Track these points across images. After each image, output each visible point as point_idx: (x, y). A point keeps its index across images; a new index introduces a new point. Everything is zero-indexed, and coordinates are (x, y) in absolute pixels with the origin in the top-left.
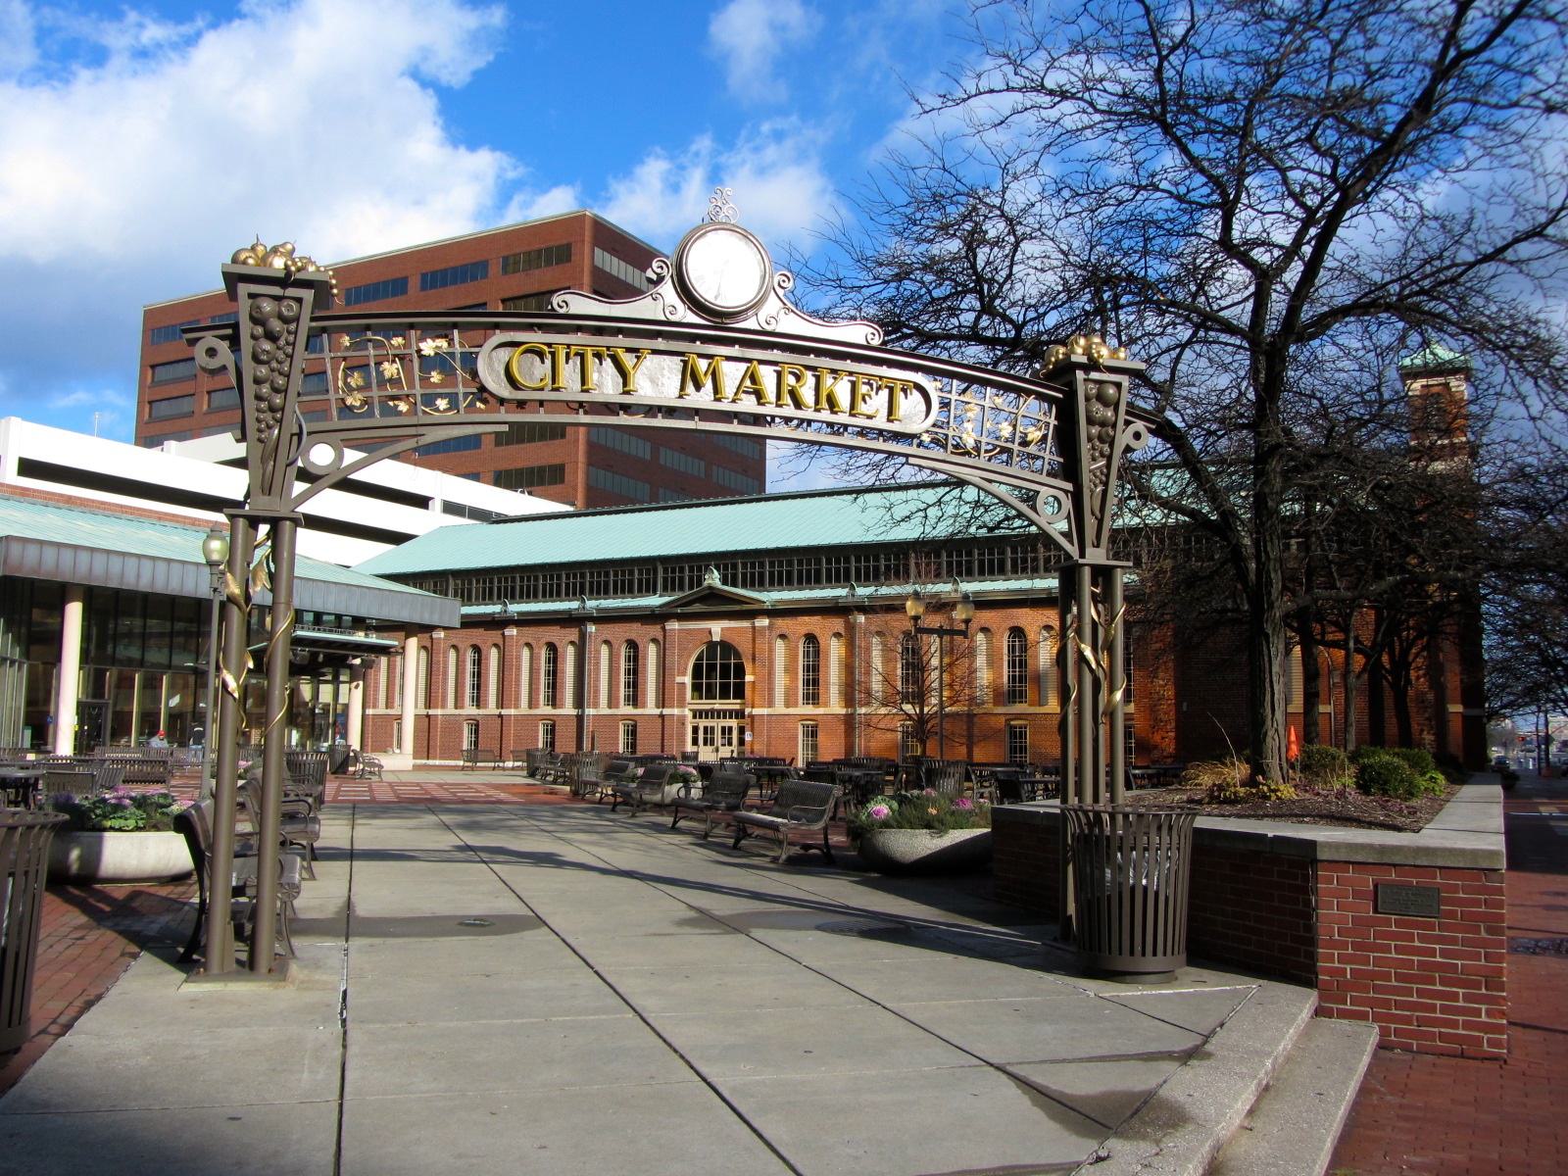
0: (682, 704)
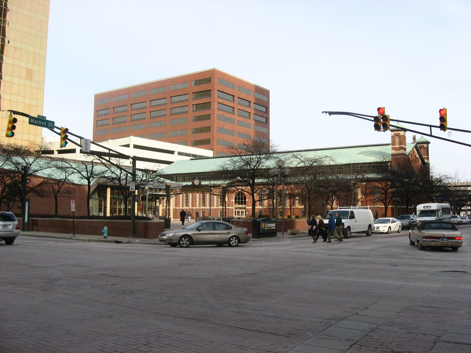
0: (232, 206)
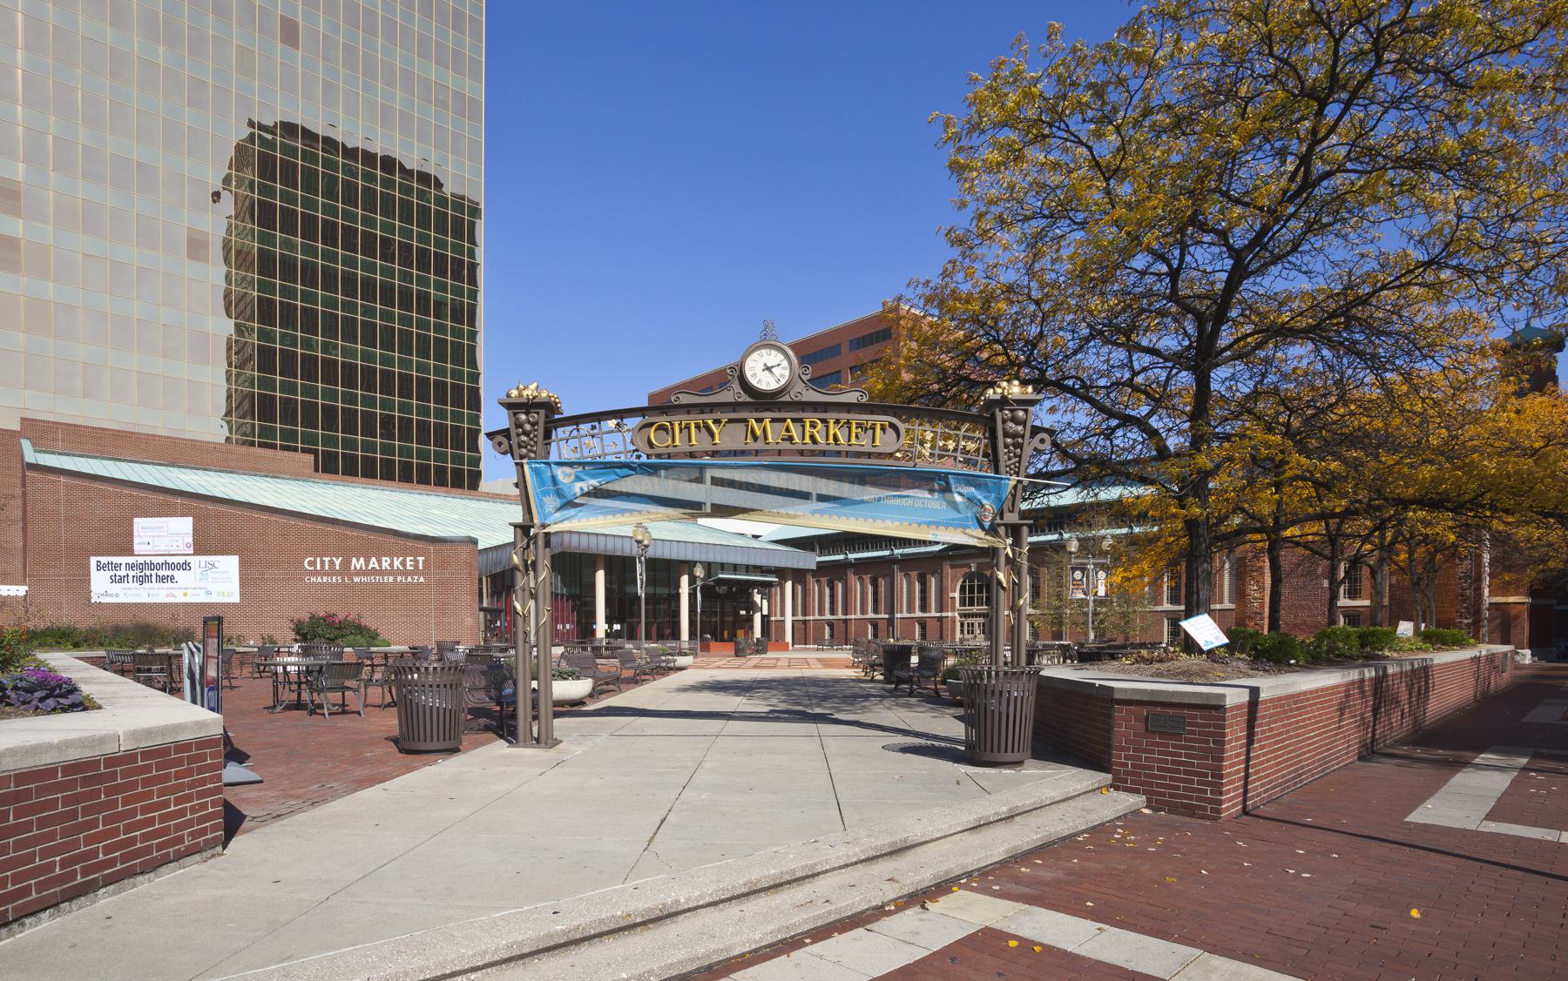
0: (953, 610)
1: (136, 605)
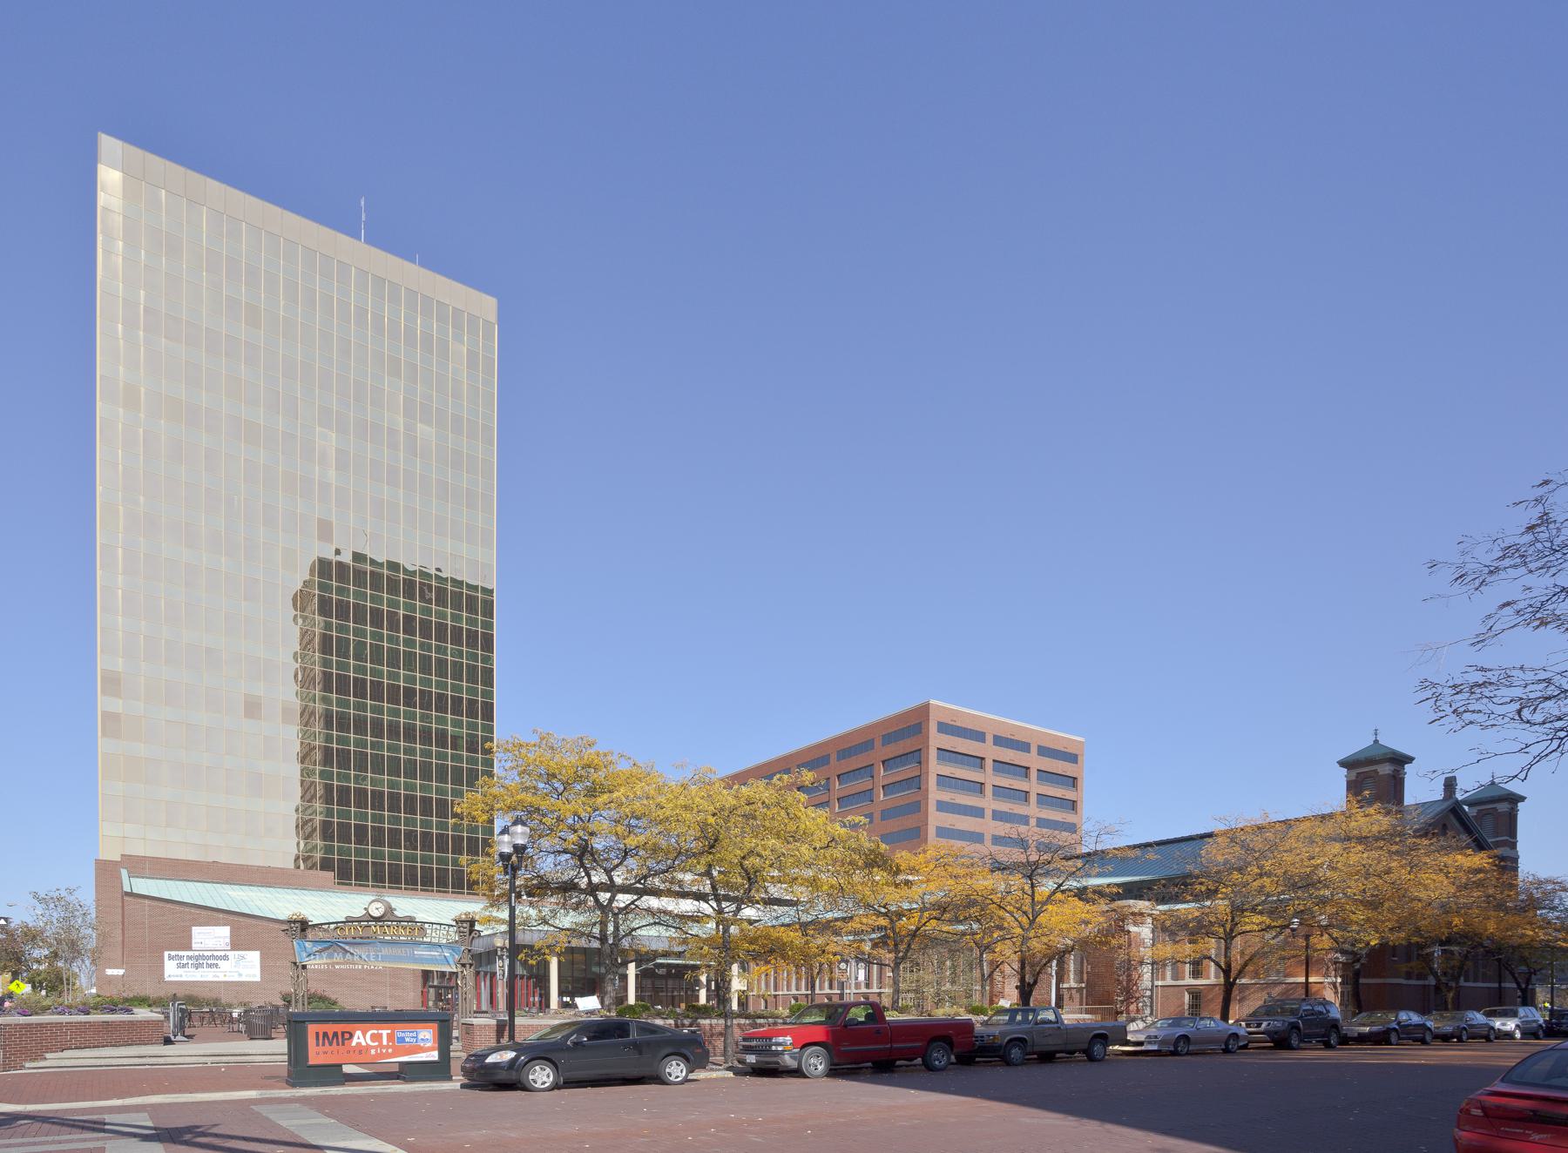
1: (193, 982)
